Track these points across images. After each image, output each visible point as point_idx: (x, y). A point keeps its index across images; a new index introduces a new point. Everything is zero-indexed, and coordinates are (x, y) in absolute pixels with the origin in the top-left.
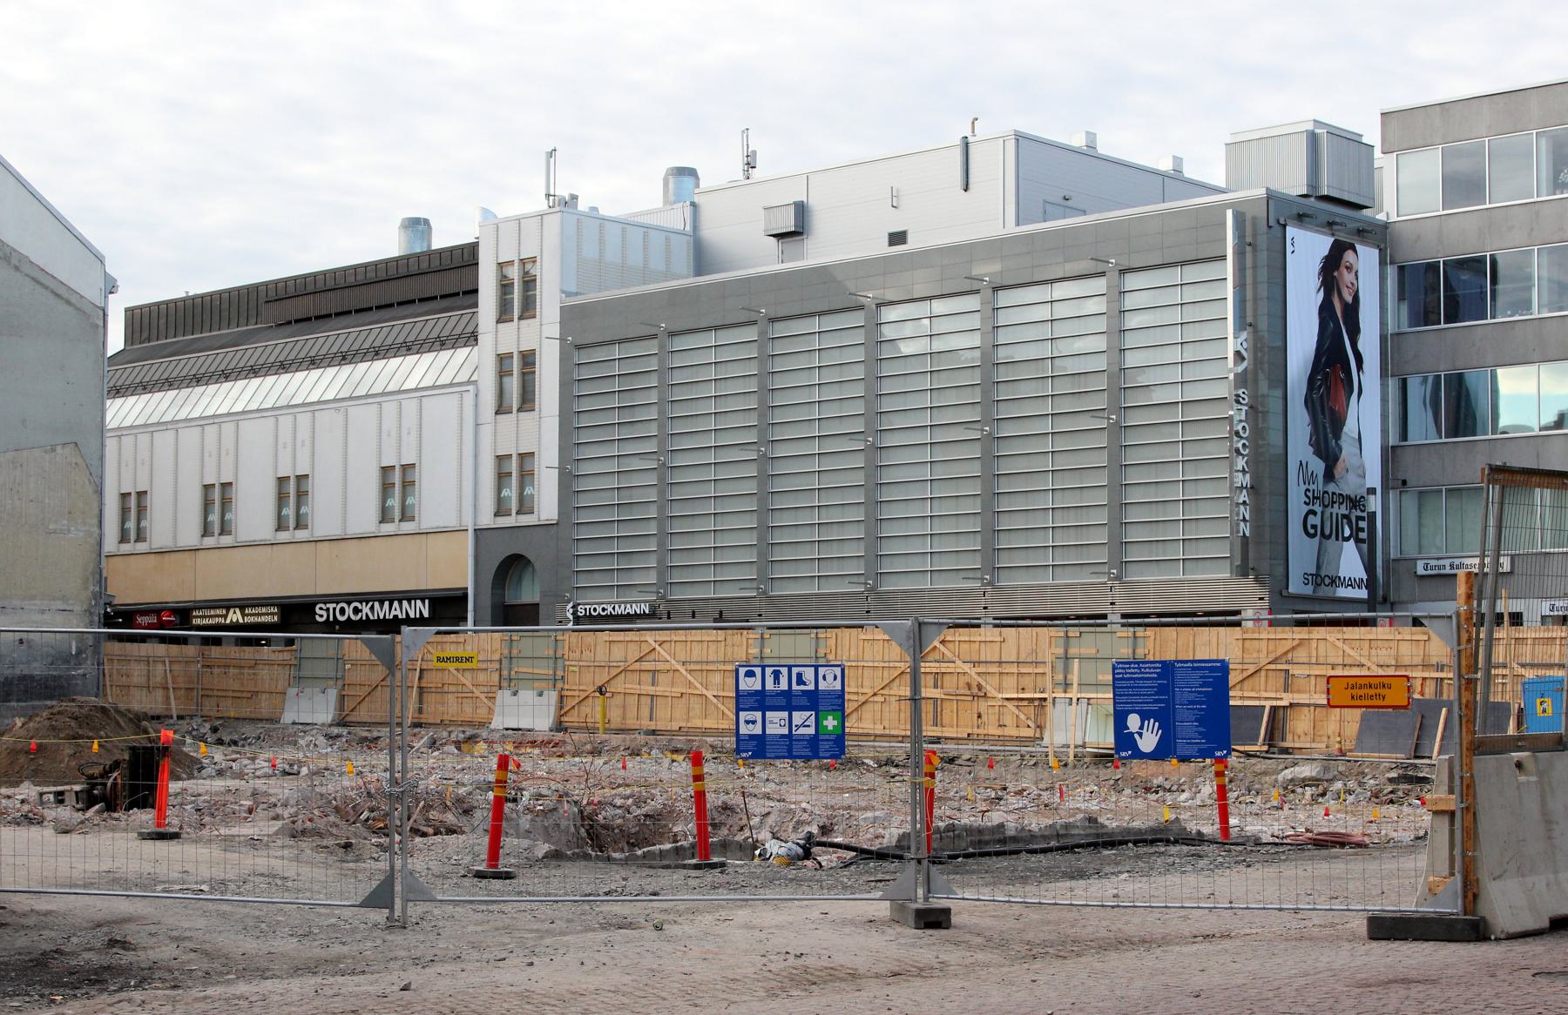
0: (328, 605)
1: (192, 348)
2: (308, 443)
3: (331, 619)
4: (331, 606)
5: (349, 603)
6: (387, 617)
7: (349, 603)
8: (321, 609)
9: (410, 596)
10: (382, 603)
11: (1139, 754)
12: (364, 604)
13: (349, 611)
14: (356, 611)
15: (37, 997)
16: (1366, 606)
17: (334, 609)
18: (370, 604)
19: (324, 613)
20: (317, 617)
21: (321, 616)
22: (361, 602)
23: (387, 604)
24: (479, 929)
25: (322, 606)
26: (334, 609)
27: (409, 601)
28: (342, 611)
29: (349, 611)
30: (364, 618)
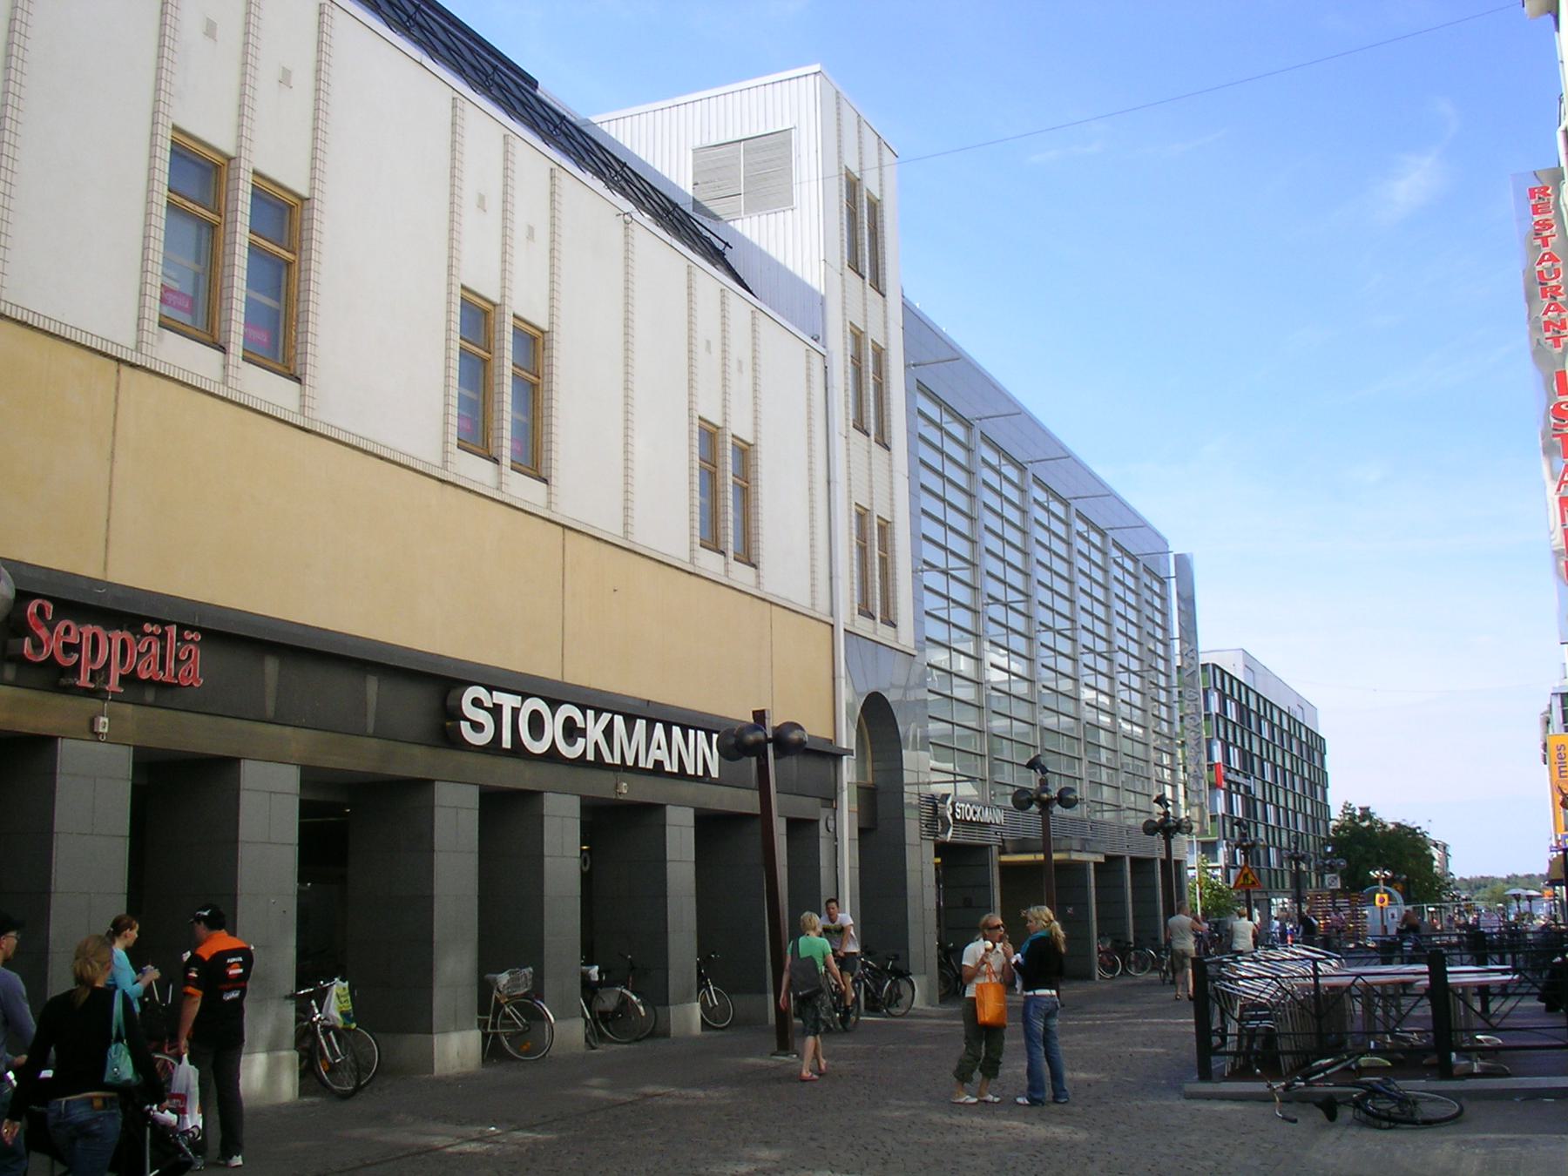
0: (499, 697)
1: (425, 40)
2: (519, 234)
3: (507, 742)
4: (508, 701)
5: (554, 704)
6: (641, 764)
7: (554, 704)
8: (477, 703)
9: (688, 722)
10: (630, 720)
11: (96, 736)
12: (590, 713)
13: (554, 728)
14: (572, 731)
15: (870, 1147)
16: (1536, 997)
17: (515, 712)
18: (606, 717)
19: (483, 717)
20: (465, 727)
21: (477, 727)
22: (583, 709)
23: (641, 725)
24: (1161, 1006)
25: (481, 692)
26: (515, 712)
27: (685, 730)
28: (536, 722)
29: (554, 728)
30: (590, 757)
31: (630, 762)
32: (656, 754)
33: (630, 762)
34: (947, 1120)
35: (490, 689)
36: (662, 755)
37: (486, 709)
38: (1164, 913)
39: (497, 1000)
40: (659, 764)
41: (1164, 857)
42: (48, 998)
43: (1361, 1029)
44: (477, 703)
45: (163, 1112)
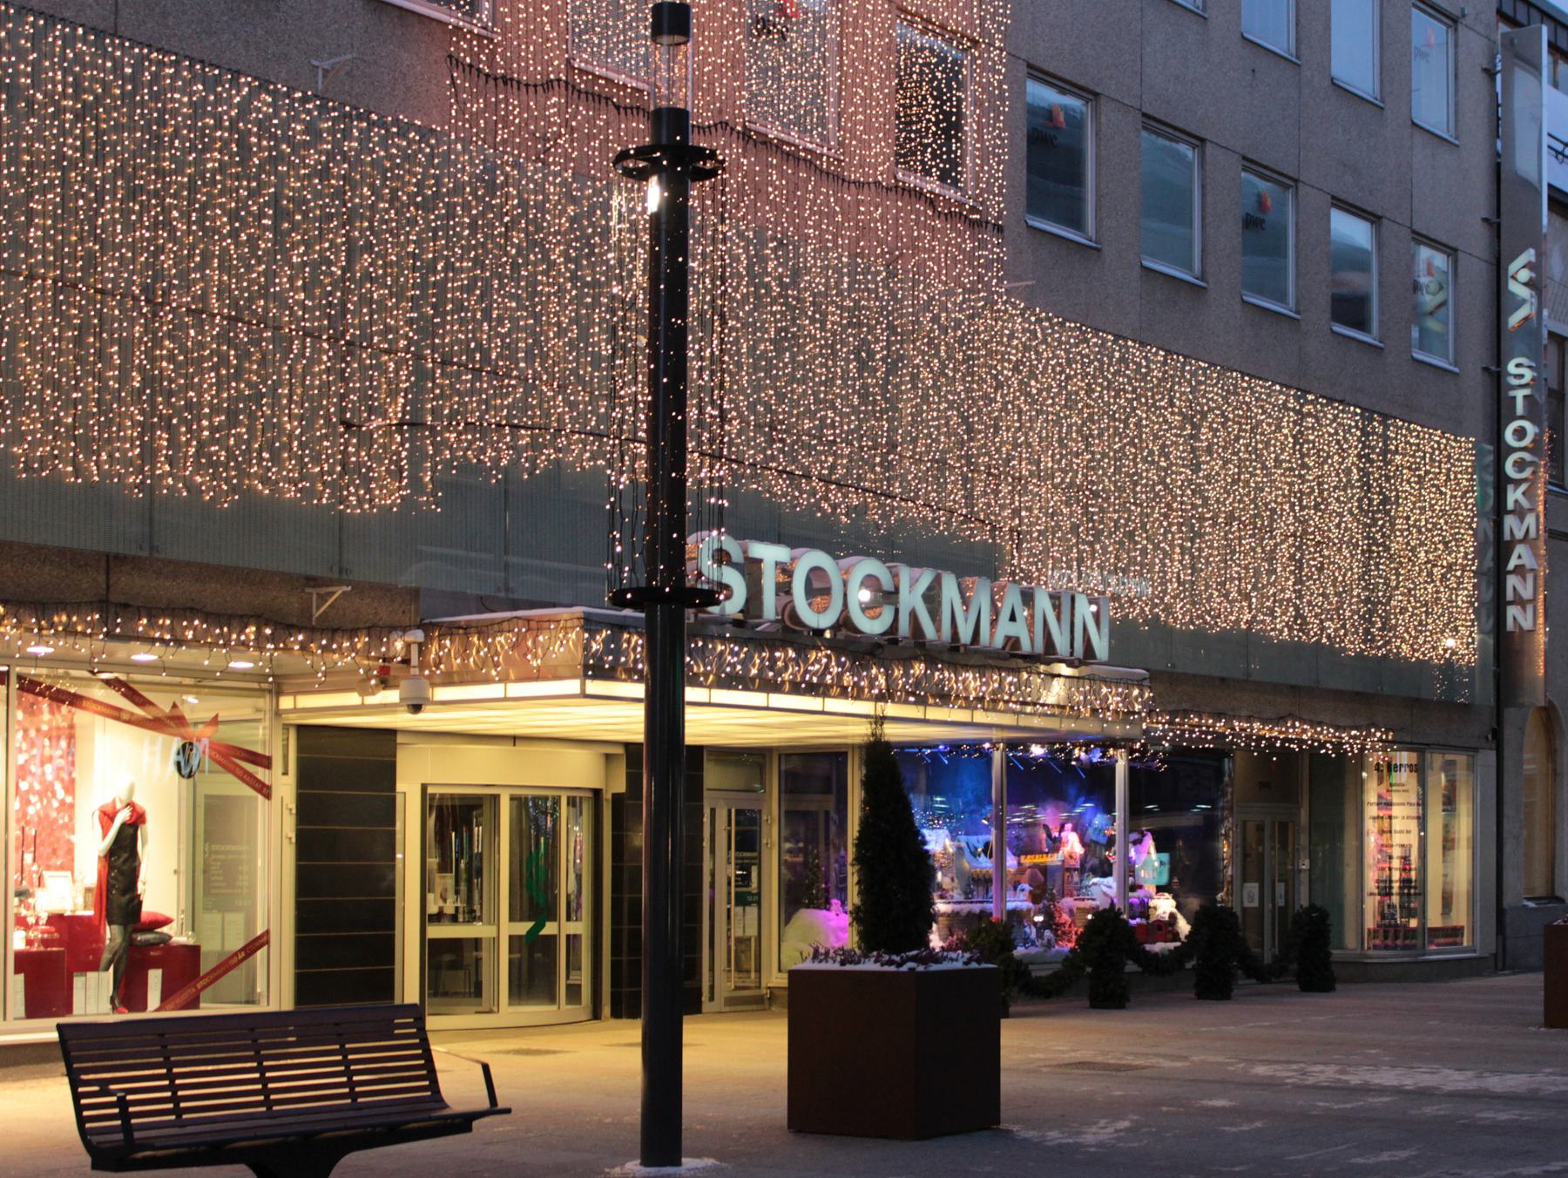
0: (759, 550)
4: (770, 554)
8: (721, 557)
17: (786, 570)
26: (786, 570)
31: (965, 635)
32: (1005, 628)
33: (965, 635)
34: (850, 857)
35: (741, 534)
36: (1019, 630)
37: (735, 566)
38: (1058, 220)
39: (1108, 807)
40: (1013, 642)
41: (1555, 386)
42: (925, 832)
43: (1544, 895)
44: (721, 557)
45: (17, 971)
